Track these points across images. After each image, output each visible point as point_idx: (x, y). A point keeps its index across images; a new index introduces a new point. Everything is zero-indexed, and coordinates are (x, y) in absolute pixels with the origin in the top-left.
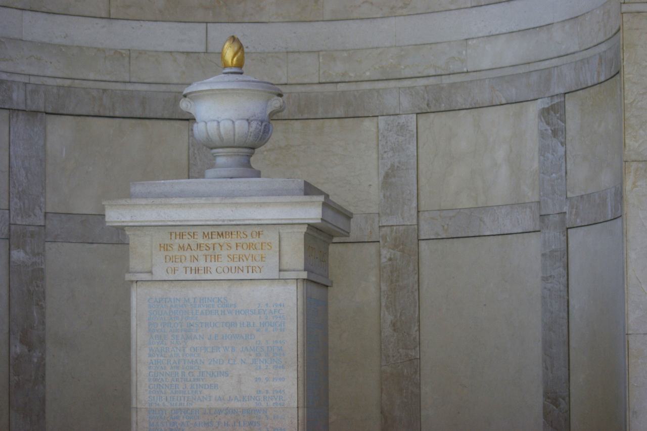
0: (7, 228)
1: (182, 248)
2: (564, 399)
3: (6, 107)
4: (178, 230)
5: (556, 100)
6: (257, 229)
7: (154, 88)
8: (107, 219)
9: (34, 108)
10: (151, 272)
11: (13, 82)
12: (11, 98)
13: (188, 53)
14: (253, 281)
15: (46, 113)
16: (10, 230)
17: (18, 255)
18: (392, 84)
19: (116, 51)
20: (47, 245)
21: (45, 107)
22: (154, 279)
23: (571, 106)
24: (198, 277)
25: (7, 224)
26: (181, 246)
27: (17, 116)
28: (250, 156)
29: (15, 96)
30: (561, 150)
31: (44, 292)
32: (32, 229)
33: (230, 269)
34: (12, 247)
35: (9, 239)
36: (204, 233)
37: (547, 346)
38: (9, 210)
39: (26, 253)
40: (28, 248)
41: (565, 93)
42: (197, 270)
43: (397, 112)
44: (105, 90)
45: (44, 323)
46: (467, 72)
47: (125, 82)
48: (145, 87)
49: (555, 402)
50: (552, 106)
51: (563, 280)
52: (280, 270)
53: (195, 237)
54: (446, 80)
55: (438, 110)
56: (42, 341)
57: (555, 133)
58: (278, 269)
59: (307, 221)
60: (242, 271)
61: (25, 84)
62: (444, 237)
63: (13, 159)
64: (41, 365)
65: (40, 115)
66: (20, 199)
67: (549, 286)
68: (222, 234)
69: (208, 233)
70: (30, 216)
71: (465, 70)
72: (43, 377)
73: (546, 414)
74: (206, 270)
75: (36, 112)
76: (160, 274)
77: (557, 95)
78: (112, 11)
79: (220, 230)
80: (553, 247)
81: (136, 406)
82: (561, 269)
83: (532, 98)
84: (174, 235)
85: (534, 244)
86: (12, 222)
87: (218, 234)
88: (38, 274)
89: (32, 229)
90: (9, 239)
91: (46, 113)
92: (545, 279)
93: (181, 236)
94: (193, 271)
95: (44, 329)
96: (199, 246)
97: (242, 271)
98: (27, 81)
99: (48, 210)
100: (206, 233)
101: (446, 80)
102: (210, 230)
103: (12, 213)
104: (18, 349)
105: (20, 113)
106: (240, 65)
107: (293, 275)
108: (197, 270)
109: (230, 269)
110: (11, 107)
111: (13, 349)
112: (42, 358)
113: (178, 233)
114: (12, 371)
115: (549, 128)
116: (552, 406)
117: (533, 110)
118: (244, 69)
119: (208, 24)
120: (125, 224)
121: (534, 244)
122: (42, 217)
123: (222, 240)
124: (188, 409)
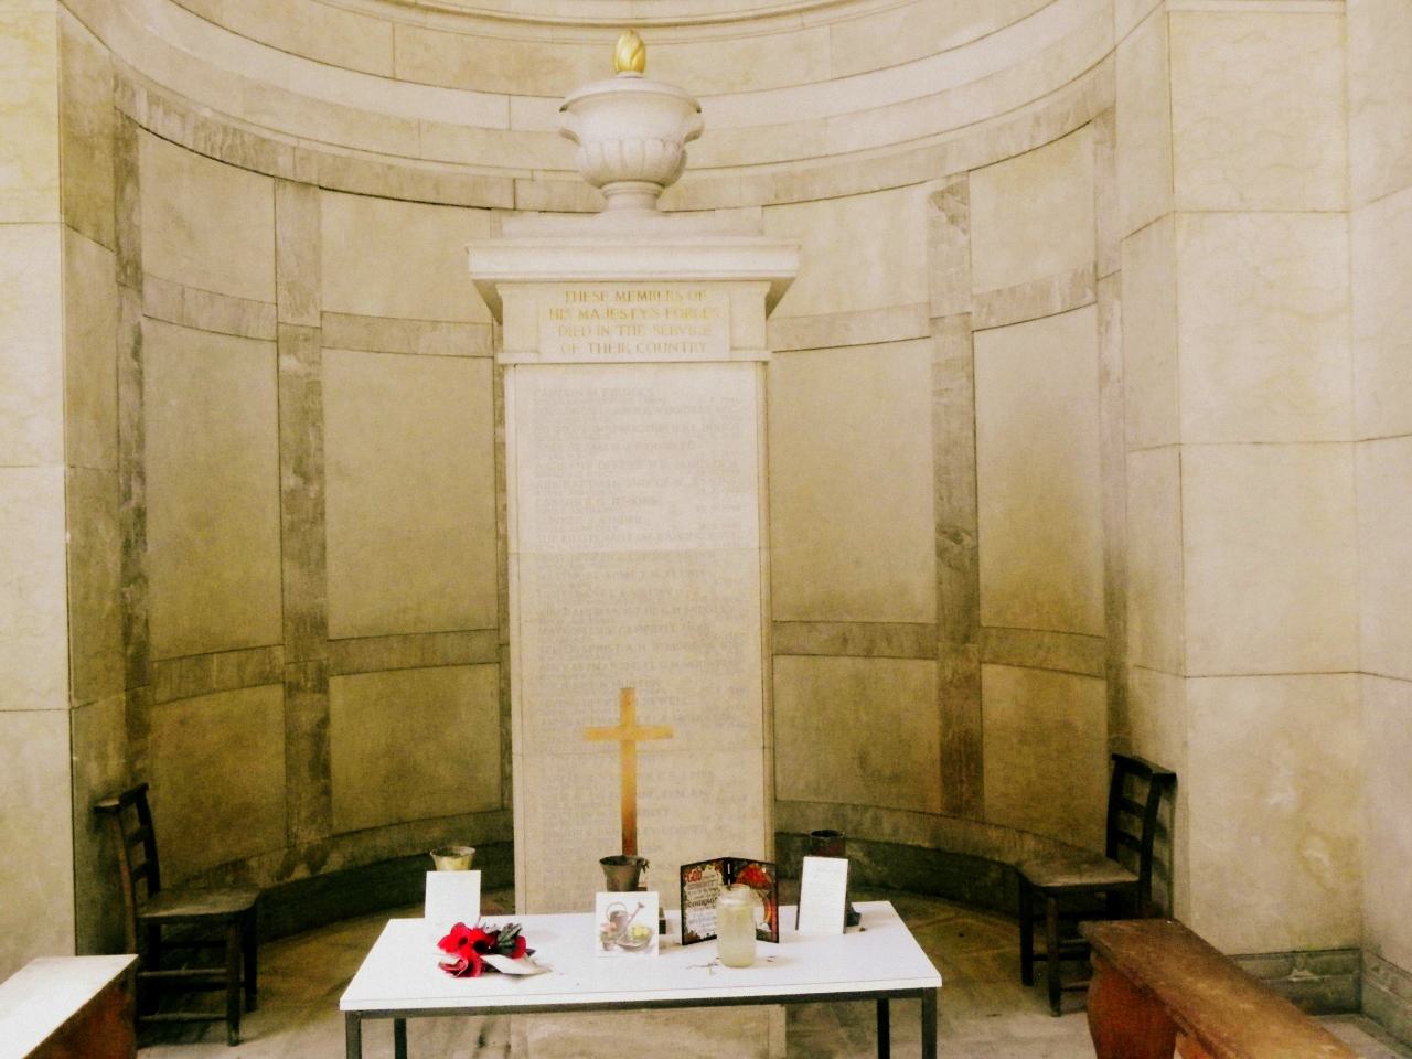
0: (274, 328)
1: (584, 315)
2: (969, 534)
3: (271, 173)
4: (577, 289)
5: (955, 180)
6: (698, 288)
7: (449, 168)
8: (471, 269)
9: (305, 179)
10: (537, 351)
11: (277, 143)
12: (275, 163)
13: (487, 129)
14: (693, 366)
15: (321, 188)
16: (277, 330)
17: (288, 362)
18: (729, 173)
19: (403, 122)
20: (325, 353)
21: (318, 181)
22: (543, 361)
23: (976, 184)
24: (609, 358)
25: (275, 322)
26: (584, 311)
27: (285, 187)
28: (657, 196)
29: (280, 160)
30: (962, 239)
31: (321, 410)
32: (303, 331)
33: (657, 347)
34: (281, 351)
35: (277, 341)
36: (617, 293)
37: (941, 473)
38: (276, 304)
39: (298, 359)
40: (301, 356)
41: (970, 171)
42: (608, 349)
43: (738, 205)
44: (390, 167)
45: (321, 450)
46: (827, 156)
47: (414, 159)
48: (440, 167)
49: (956, 537)
50: (949, 188)
51: (967, 393)
52: (732, 349)
53: (605, 298)
54: (799, 167)
55: (790, 201)
56: (320, 472)
57: (953, 220)
58: (728, 347)
59: (769, 275)
60: (676, 349)
61: (294, 148)
62: (798, 348)
63: (280, 241)
64: (320, 502)
65: (312, 189)
66: (289, 291)
67: (945, 400)
68: (645, 294)
69: (624, 294)
70: (302, 315)
71: (824, 153)
72: (322, 514)
73: (941, 552)
74: (621, 348)
75: (308, 185)
76: (551, 353)
77: (956, 174)
78: (397, 71)
79: (641, 288)
80: (951, 354)
81: (516, 551)
82: (964, 380)
83: (917, 180)
84: (571, 296)
85: (922, 355)
86: (280, 320)
87: (639, 294)
88: (313, 388)
89: (303, 331)
90: (277, 341)
91: (321, 188)
92: (938, 393)
93: (583, 297)
94: (602, 350)
95: (322, 456)
96: (610, 313)
97: (676, 349)
98: (295, 144)
99: (325, 309)
100: (621, 294)
101: (799, 167)
102: (627, 288)
103: (280, 308)
104: (291, 481)
105: (288, 183)
106: (641, 68)
107: (752, 355)
108: (608, 349)
109: (657, 347)
110: (278, 175)
111: (285, 482)
112: (321, 493)
113: (578, 293)
114: (284, 509)
115: (943, 214)
116: (948, 541)
117: (920, 195)
118: (645, 73)
119: (512, 98)
120: (499, 277)
121: (922, 355)
122: (318, 317)
123: (645, 304)
124: (597, 554)
